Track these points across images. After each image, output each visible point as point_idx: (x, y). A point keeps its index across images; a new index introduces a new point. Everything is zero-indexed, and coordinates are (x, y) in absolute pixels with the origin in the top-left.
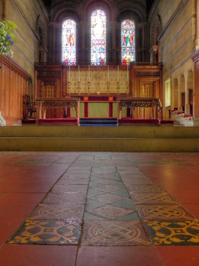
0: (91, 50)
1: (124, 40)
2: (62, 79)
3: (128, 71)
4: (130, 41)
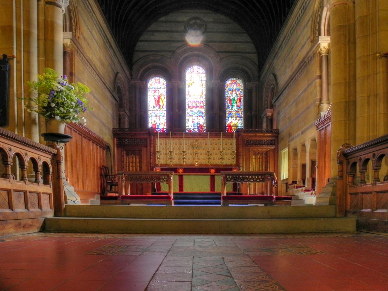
0: (187, 113)
1: (229, 102)
2: (149, 147)
3: (234, 139)
4: (237, 104)
